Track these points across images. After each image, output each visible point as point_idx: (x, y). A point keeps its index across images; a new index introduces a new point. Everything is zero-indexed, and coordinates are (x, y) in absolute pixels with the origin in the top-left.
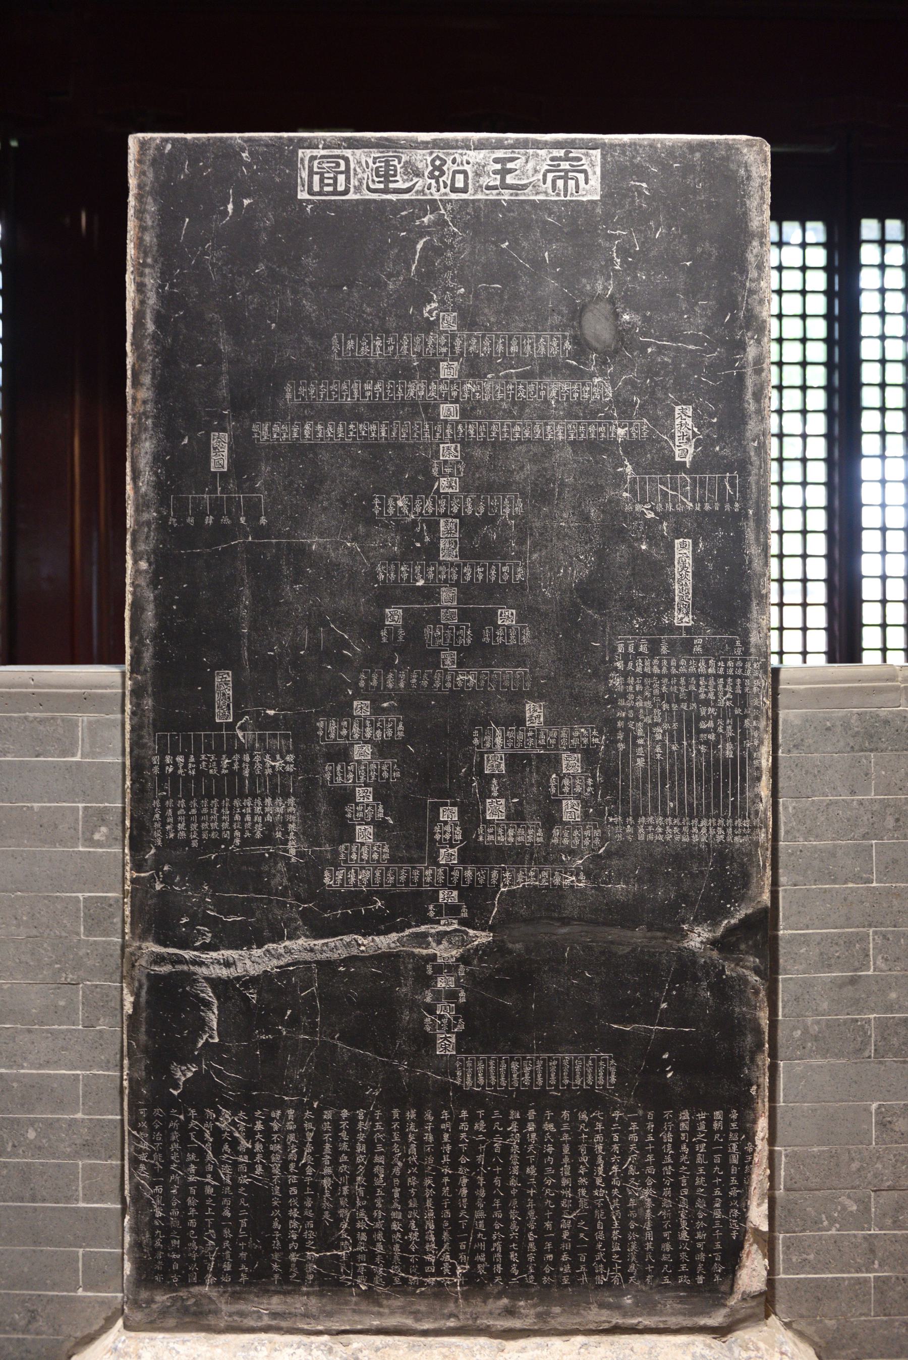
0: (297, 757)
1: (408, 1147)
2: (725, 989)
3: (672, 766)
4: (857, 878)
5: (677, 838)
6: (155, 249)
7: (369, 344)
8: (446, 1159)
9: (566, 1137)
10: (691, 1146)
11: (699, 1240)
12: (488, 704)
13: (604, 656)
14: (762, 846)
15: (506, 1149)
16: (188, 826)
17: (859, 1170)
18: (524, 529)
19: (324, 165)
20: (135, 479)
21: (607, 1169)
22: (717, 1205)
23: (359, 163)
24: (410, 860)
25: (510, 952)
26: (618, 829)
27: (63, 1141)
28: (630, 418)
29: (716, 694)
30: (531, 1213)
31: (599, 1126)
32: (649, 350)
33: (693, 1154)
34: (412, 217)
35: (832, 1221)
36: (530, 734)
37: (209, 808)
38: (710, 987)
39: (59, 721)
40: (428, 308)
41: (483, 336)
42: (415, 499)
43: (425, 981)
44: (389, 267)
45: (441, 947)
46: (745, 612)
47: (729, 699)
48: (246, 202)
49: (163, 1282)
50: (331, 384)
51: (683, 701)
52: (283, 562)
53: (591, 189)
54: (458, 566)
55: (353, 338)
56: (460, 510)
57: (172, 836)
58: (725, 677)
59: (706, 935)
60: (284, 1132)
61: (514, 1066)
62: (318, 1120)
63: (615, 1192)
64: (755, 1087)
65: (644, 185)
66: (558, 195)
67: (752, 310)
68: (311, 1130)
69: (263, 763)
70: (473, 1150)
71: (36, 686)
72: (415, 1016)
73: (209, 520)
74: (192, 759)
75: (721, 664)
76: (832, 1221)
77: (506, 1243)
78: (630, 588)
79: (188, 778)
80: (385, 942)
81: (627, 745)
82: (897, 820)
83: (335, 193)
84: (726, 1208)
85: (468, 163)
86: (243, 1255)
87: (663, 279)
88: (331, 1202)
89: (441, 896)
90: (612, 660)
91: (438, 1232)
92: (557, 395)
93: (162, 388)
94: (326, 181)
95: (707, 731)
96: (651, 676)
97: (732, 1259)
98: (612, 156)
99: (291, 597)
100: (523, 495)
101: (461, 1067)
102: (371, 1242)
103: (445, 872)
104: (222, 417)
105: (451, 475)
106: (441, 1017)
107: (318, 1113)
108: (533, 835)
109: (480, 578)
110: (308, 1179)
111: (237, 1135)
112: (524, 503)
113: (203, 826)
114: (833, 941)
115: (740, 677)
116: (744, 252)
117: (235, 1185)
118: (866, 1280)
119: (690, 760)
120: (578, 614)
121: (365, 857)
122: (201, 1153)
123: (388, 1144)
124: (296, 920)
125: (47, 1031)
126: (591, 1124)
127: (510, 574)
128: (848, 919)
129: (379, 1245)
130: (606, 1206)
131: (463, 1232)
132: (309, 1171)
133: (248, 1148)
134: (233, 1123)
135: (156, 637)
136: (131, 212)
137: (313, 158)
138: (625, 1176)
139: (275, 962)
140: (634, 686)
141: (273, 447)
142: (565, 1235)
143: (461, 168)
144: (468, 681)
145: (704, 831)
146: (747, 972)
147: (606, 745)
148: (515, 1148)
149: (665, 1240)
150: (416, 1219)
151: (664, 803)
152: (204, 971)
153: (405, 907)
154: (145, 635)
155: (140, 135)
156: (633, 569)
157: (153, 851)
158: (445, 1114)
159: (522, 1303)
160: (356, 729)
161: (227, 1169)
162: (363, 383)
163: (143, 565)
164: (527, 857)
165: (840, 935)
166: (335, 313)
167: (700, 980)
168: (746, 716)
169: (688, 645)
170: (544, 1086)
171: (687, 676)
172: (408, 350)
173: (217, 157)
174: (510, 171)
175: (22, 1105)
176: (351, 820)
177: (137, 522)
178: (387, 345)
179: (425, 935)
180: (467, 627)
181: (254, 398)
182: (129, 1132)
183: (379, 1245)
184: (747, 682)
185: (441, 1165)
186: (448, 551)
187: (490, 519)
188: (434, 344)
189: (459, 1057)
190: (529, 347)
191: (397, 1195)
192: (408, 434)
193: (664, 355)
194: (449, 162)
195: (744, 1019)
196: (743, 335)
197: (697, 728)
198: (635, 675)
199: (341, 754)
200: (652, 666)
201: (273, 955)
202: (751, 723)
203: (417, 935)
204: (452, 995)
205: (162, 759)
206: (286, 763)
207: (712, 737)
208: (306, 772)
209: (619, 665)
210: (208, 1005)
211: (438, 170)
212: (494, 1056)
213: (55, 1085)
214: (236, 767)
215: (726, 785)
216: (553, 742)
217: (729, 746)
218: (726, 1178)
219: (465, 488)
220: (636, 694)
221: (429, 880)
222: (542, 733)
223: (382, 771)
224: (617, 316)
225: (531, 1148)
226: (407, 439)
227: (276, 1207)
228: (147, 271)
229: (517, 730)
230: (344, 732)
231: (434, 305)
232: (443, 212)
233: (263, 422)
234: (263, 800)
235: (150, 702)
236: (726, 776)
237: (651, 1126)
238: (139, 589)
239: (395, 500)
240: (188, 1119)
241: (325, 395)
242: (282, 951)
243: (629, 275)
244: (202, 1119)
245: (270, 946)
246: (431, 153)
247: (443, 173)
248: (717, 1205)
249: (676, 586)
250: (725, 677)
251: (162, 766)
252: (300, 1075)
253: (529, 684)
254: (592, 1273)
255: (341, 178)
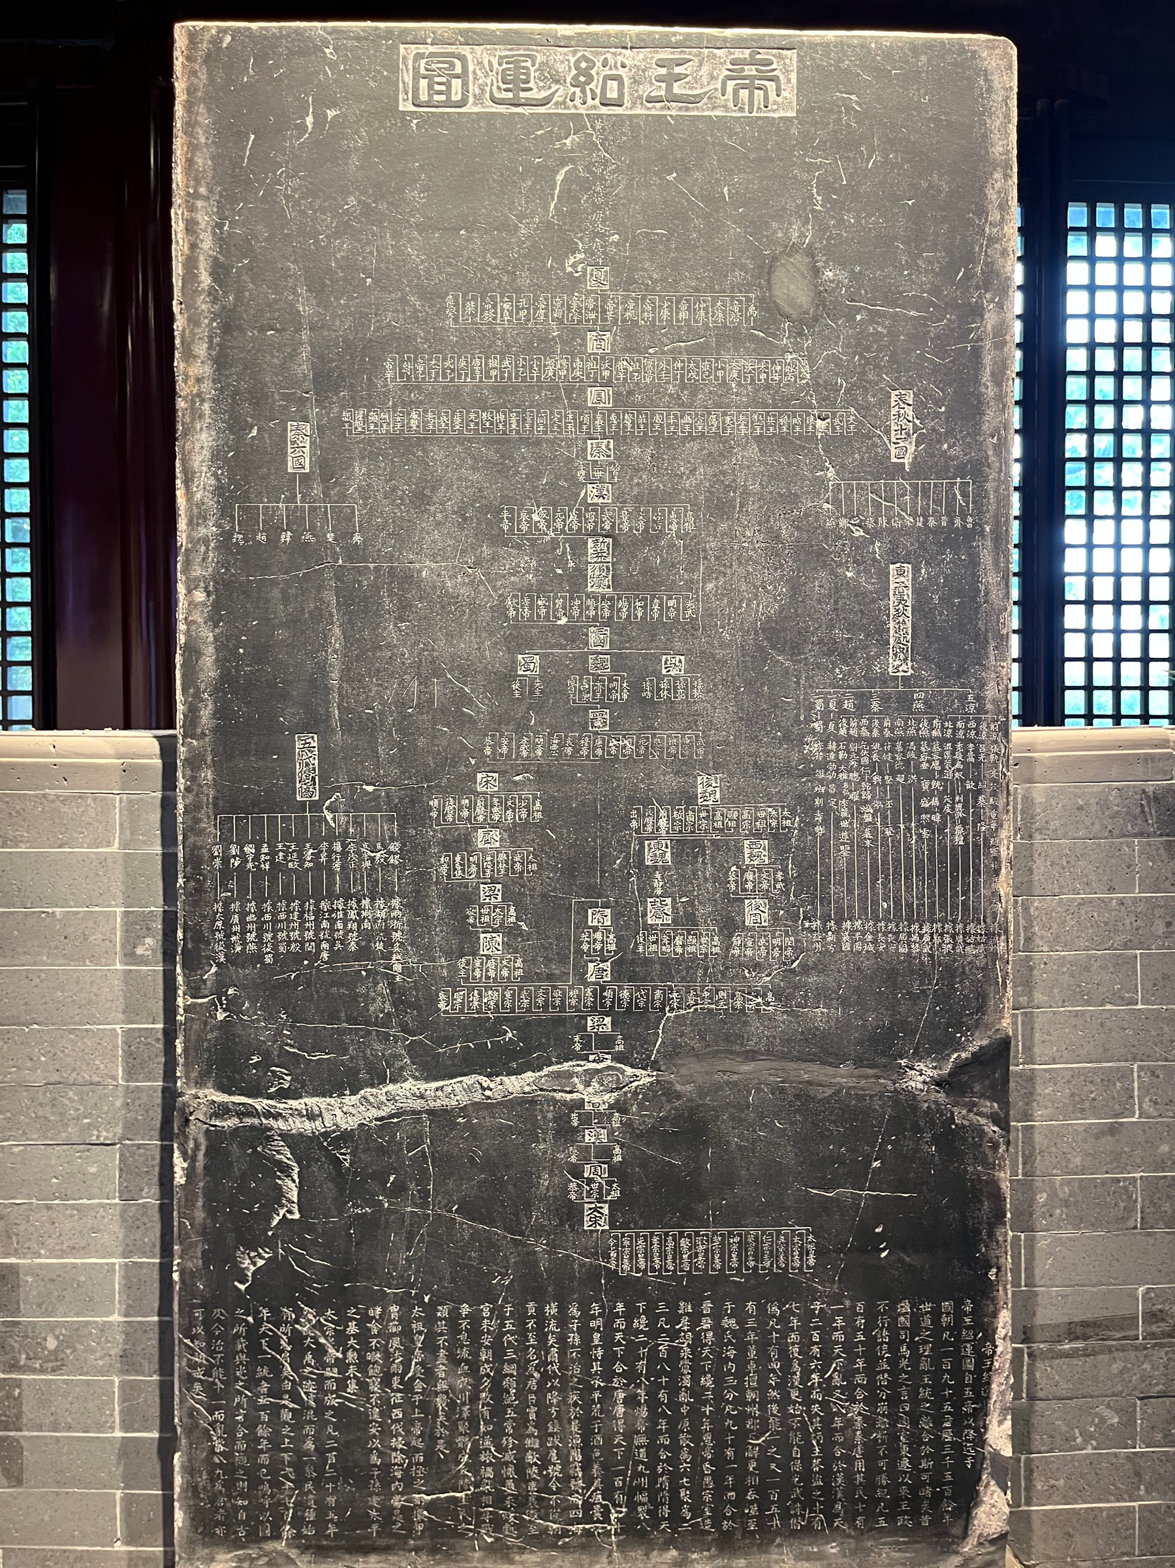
0: (404, 845)
1: (547, 1352)
2: (953, 1141)
3: (885, 855)
4: (1117, 999)
5: (892, 948)
6: (210, 174)
7: (494, 307)
8: (596, 1367)
9: (752, 1336)
10: (913, 1346)
11: (924, 1470)
12: (649, 776)
13: (798, 715)
14: (1002, 958)
15: (674, 1352)
16: (259, 936)
17: (1121, 1372)
18: (695, 550)
19: (434, 66)
20: (187, 482)
21: (805, 1377)
22: (947, 1425)
23: (480, 63)
24: (550, 977)
25: (679, 1096)
26: (815, 937)
27: (93, 1351)
28: (833, 405)
29: (942, 763)
30: (707, 1438)
31: (795, 1323)
32: (859, 317)
33: (915, 1358)
34: (550, 137)
35: (1088, 1437)
36: (704, 814)
37: (288, 912)
38: (935, 1140)
39: (89, 801)
40: (572, 260)
41: (644, 298)
42: (555, 512)
43: (566, 1134)
44: (521, 204)
45: (590, 1089)
46: (979, 658)
47: (958, 770)
48: (331, 114)
49: (227, 1535)
50: (445, 359)
51: (900, 772)
52: (384, 592)
53: (783, 102)
54: (611, 599)
55: (474, 298)
56: (613, 527)
57: (238, 949)
58: (954, 741)
59: (930, 1073)
60: (386, 1336)
61: (684, 1243)
62: (430, 1319)
63: (816, 1408)
64: (994, 1270)
65: (853, 97)
66: (741, 110)
67: (992, 263)
68: (420, 1333)
69: (359, 854)
70: (631, 1356)
71: (58, 756)
72: (556, 1180)
73: (286, 537)
74: (265, 849)
75: (948, 724)
76: (1088, 1437)
77: (675, 1477)
78: (832, 627)
79: (259, 874)
80: (516, 1084)
81: (828, 828)
82: (1169, 924)
83: (448, 104)
84: (958, 1429)
85: (623, 66)
86: (331, 1500)
87: (875, 223)
88: (446, 1427)
89: (590, 1023)
90: (808, 720)
91: (586, 1465)
92: (739, 376)
93: (221, 362)
94: (437, 87)
95: (930, 811)
96: (859, 739)
97: (967, 1498)
98: (812, 59)
99: (394, 638)
100: (695, 505)
101: (616, 1245)
102: (500, 1480)
103: (594, 992)
104: (302, 402)
105: (602, 481)
106: (590, 1181)
107: (430, 1309)
108: (707, 944)
109: (639, 614)
110: (417, 1398)
111: (322, 1340)
112: (697, 517)
113: (282, 935)
114: (1086, 1077)
115: (972, 741)
116: (982, 189)
117: (321, 1408)
118: (1131, 1510)
119: (908, 848)
120: (765, 660)
121: (492, 973)
122: (276, 1367)
123: (523, 1348)
124: (398, 1057)
125: (73, 1207)
126: (784, 1319)
127: (677, 609)
128: (1106, 1050)
129: (510, 1483)
130: (804, 1426)
131: (619, 1463)
132: (419, 1386)
133: (337, 1359)
134: (319, 1326)
135: (218, 690)
136: (178, 124)
137: (419, 56)
138: (827, 1388)
139: (375, 1113)
140: (837, 752)
141: (370, 442)
142: (752, 1466)
143: (614, 72)
144: (624, 747)
145: (927, 938)
146: (983, 1121)
147: (800, 829)
148: (686, 1352)
149: (881, 1471)
150: (557, 1448)
151: (875, 903)
152: (281, 1124)
153: (541, 1037)
154: (203, 687)
155: (190, 24)
156: (836, 602)
157: (214, 970)
158: (596, 1309)
159: (695, 1556)
160: (480, 810)
161: (310, 1387)
162: (487, 358)
163: (199, 596)
164: (700, 972)
165: (1094, 1071)
166: (450, 264)
167: (921, 1131)
168: (979, 792)
169: (904, 703)
170: (722, 1269)
171: (905, 741)
172: (546, 315)
173: (291, 53)
174: (679, 78)
175: (39, 1305)
176: (474, 926)
177: (190, 538)
178: (518, 309)
179: (569, 1075)
180: (623, 678)
181: (342, 375)
182: (180, 1340)
183: (510, 1483)
184: (983, 748)
185: (591, 1375)
186: (598, 582)
187: (651, 537)
188: (580, 308)
189: (614, 1232)
190: (702, 313)
191: (532, 1417)
192: (545, 426)
193: (878, 323)
194: (599, 64)
195: (980, 1180)
196: (980, 297)
197: (918, 806)
198: (838, 740)
199: (460, 843)
200: (859, 728)
201: (371, 1104)
202: (987, 800)
203: (558, 1075)
204: (604, 1153)
205: (226, 849)
206: (390, 853)
207: (937, 818)
208: (416, 864)
209: (817, 726)
210: (286, 1170)
211: (583, 77)
212: (657, 1231)
213: (83, 1278)
214: (323, 859)
215: (955, 880)
216: (733, 824)
217: (959, 829)
218: (960, 1387)
219: (620, 498)
220: (839, 763)
221: (573, 1002)
222: (718, 813)
223: (514, 863)
224: (816, 272)
225: (706, 1351)
226: (545, 432)
227: (374, 1436)
228: (199, 204)
229: (686, 810)
230: (466, 813)
231: (579, 256)
232: (590, 131)
233: (356, 408)
234: (359, 902)
235: (210, 776)
236: (955, 867)
237: (861, 1322)
238: (193, 627)
239: (530, 512)
240: (259, 1322)
241: (437, 374)
242: (383, 1098)
243: (833, 217)
244: (277, 1321)
245: (367, 1091)
246: (574, 53)
247: (590, 79)
248: (947, 1425)
249: (892, 625)
250: (954, 741)
251: (226, 860)
252: (407, 1259)
253: (701, 751)
254: (785, 1516)
255: (456, 84)
